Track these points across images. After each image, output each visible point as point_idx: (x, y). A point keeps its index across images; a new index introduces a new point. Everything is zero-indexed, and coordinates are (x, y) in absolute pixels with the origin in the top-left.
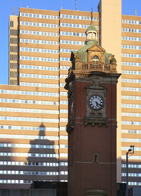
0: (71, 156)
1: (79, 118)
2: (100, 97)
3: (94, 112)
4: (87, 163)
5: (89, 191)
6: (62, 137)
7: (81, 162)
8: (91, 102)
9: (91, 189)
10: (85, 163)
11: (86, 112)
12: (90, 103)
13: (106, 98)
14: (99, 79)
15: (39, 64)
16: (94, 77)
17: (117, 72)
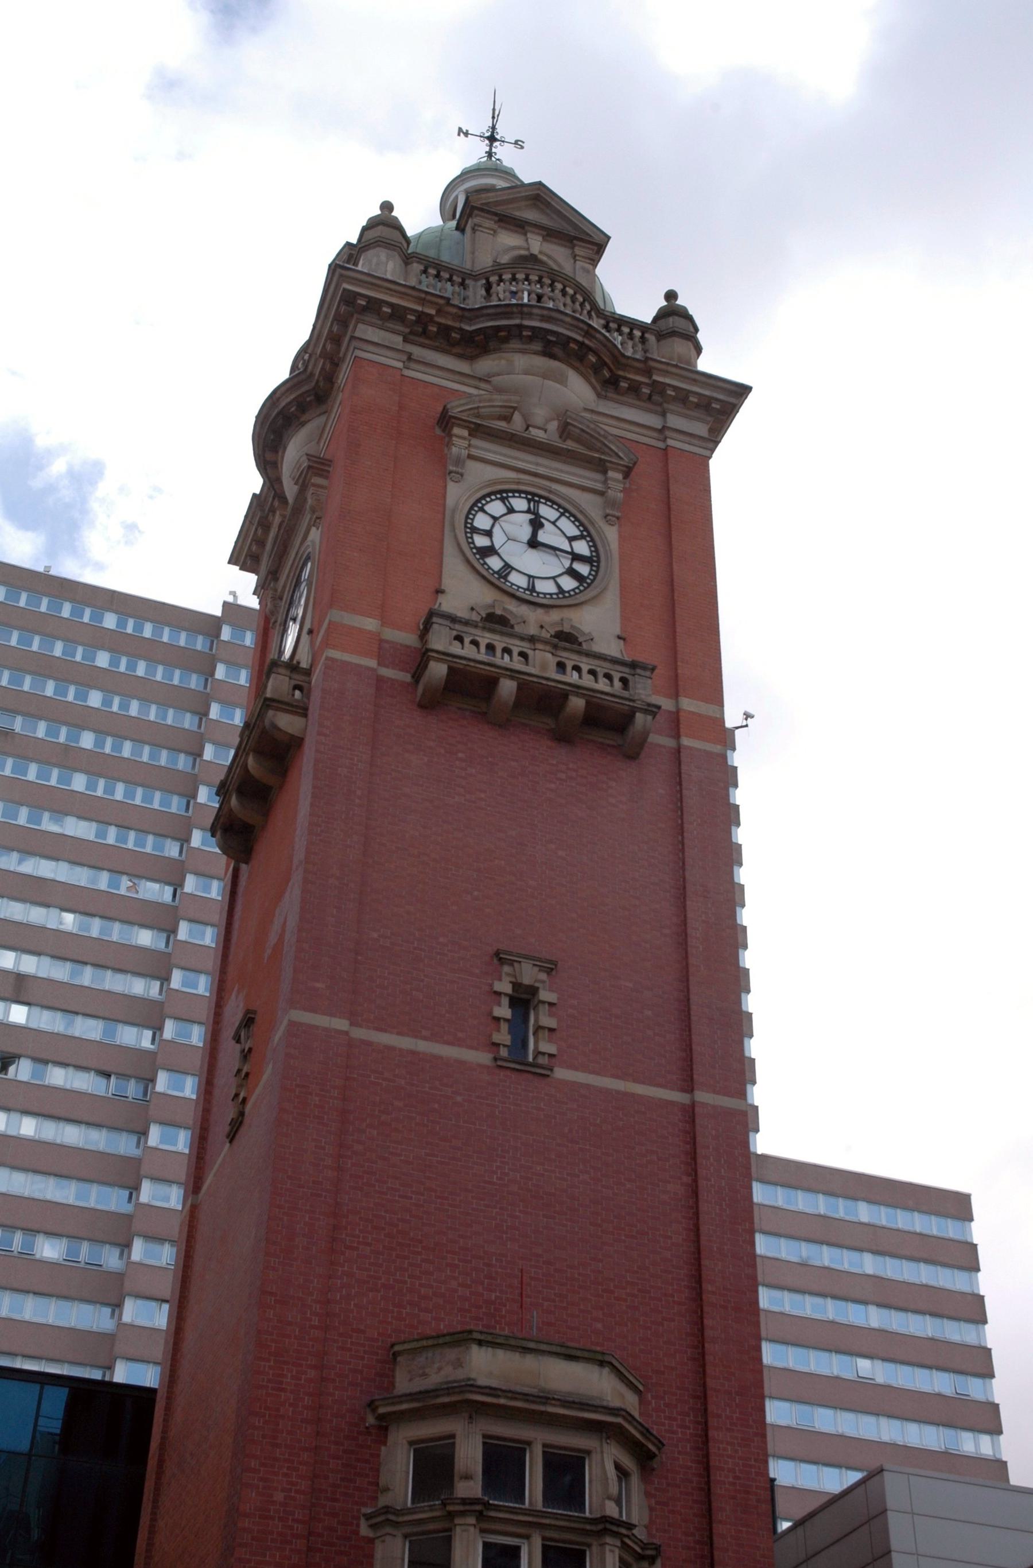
0: (310, 632)
1: (370, 624)
2: (564, 512)
3: (512, 606)
4: (423, 1046)
5: (438, 1371)
6: (132, 1311)
7: (360, 1033)
8: (489, 533)
9: (462, 1339)
10: (406, 1043)
11: (439, 591)
12: (481, 541)
13: (622, 538)
14: (562, 381)
15: (81, 719)
16: (521, 361)
17: (698, 350)
